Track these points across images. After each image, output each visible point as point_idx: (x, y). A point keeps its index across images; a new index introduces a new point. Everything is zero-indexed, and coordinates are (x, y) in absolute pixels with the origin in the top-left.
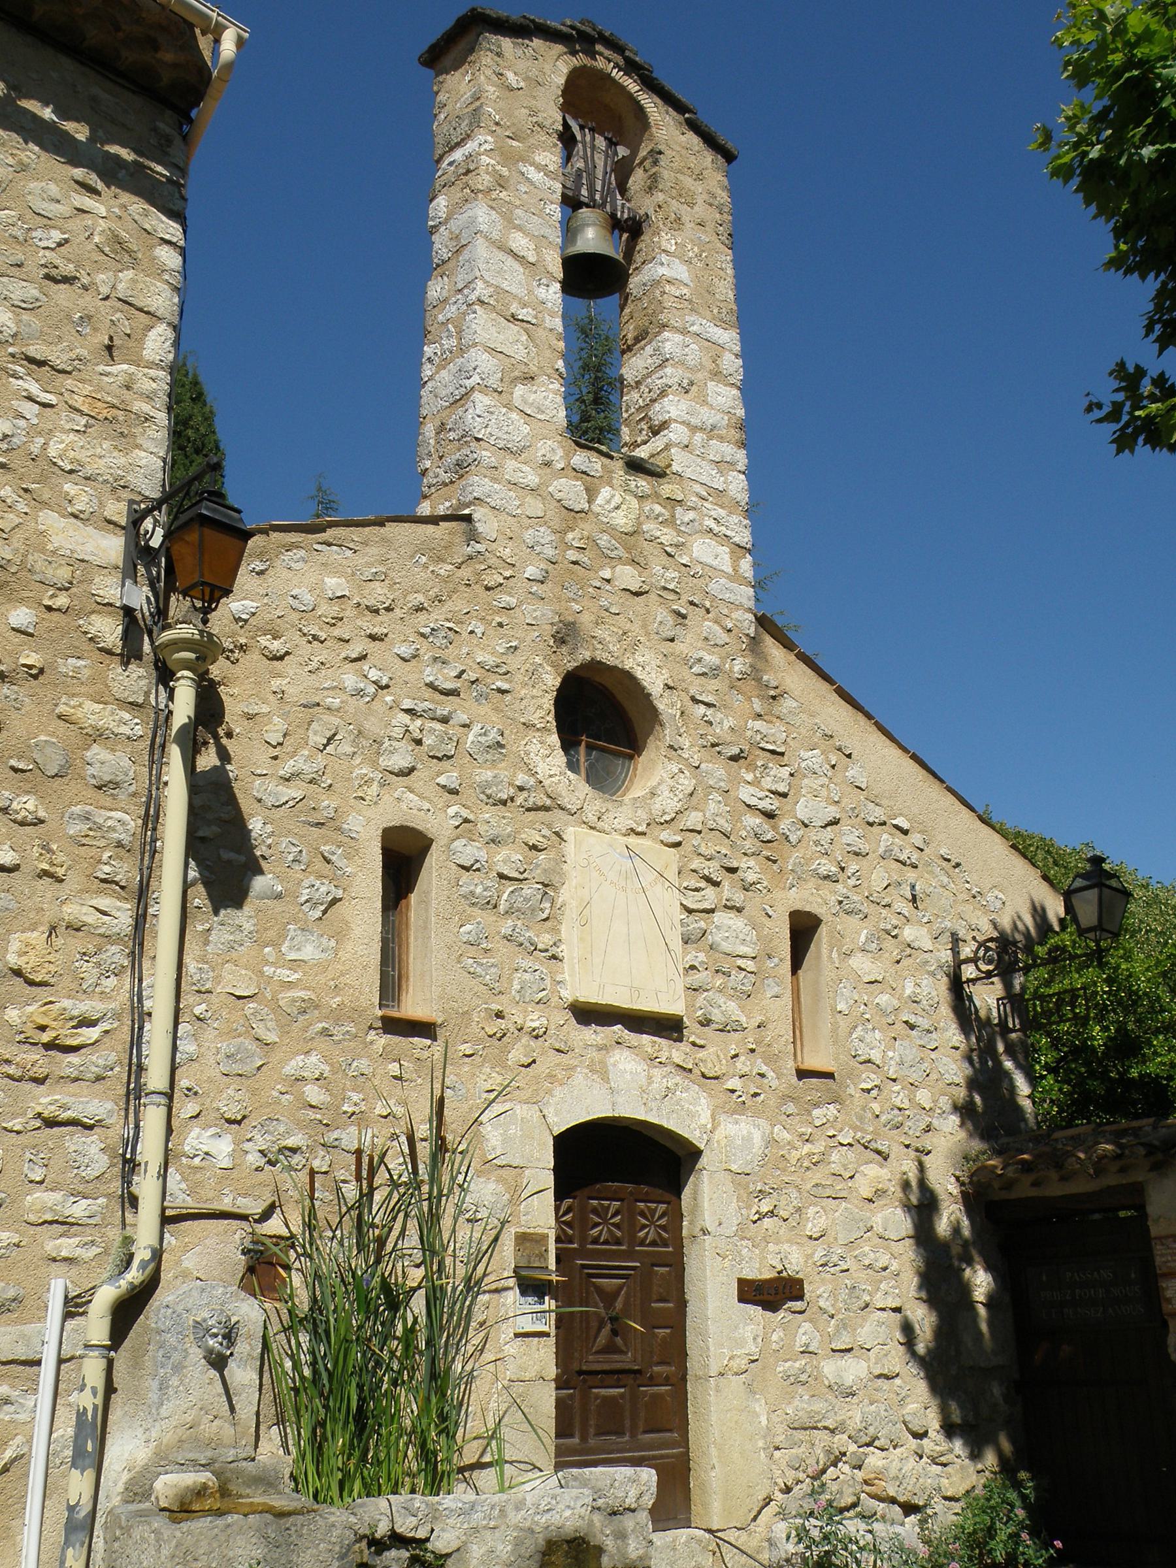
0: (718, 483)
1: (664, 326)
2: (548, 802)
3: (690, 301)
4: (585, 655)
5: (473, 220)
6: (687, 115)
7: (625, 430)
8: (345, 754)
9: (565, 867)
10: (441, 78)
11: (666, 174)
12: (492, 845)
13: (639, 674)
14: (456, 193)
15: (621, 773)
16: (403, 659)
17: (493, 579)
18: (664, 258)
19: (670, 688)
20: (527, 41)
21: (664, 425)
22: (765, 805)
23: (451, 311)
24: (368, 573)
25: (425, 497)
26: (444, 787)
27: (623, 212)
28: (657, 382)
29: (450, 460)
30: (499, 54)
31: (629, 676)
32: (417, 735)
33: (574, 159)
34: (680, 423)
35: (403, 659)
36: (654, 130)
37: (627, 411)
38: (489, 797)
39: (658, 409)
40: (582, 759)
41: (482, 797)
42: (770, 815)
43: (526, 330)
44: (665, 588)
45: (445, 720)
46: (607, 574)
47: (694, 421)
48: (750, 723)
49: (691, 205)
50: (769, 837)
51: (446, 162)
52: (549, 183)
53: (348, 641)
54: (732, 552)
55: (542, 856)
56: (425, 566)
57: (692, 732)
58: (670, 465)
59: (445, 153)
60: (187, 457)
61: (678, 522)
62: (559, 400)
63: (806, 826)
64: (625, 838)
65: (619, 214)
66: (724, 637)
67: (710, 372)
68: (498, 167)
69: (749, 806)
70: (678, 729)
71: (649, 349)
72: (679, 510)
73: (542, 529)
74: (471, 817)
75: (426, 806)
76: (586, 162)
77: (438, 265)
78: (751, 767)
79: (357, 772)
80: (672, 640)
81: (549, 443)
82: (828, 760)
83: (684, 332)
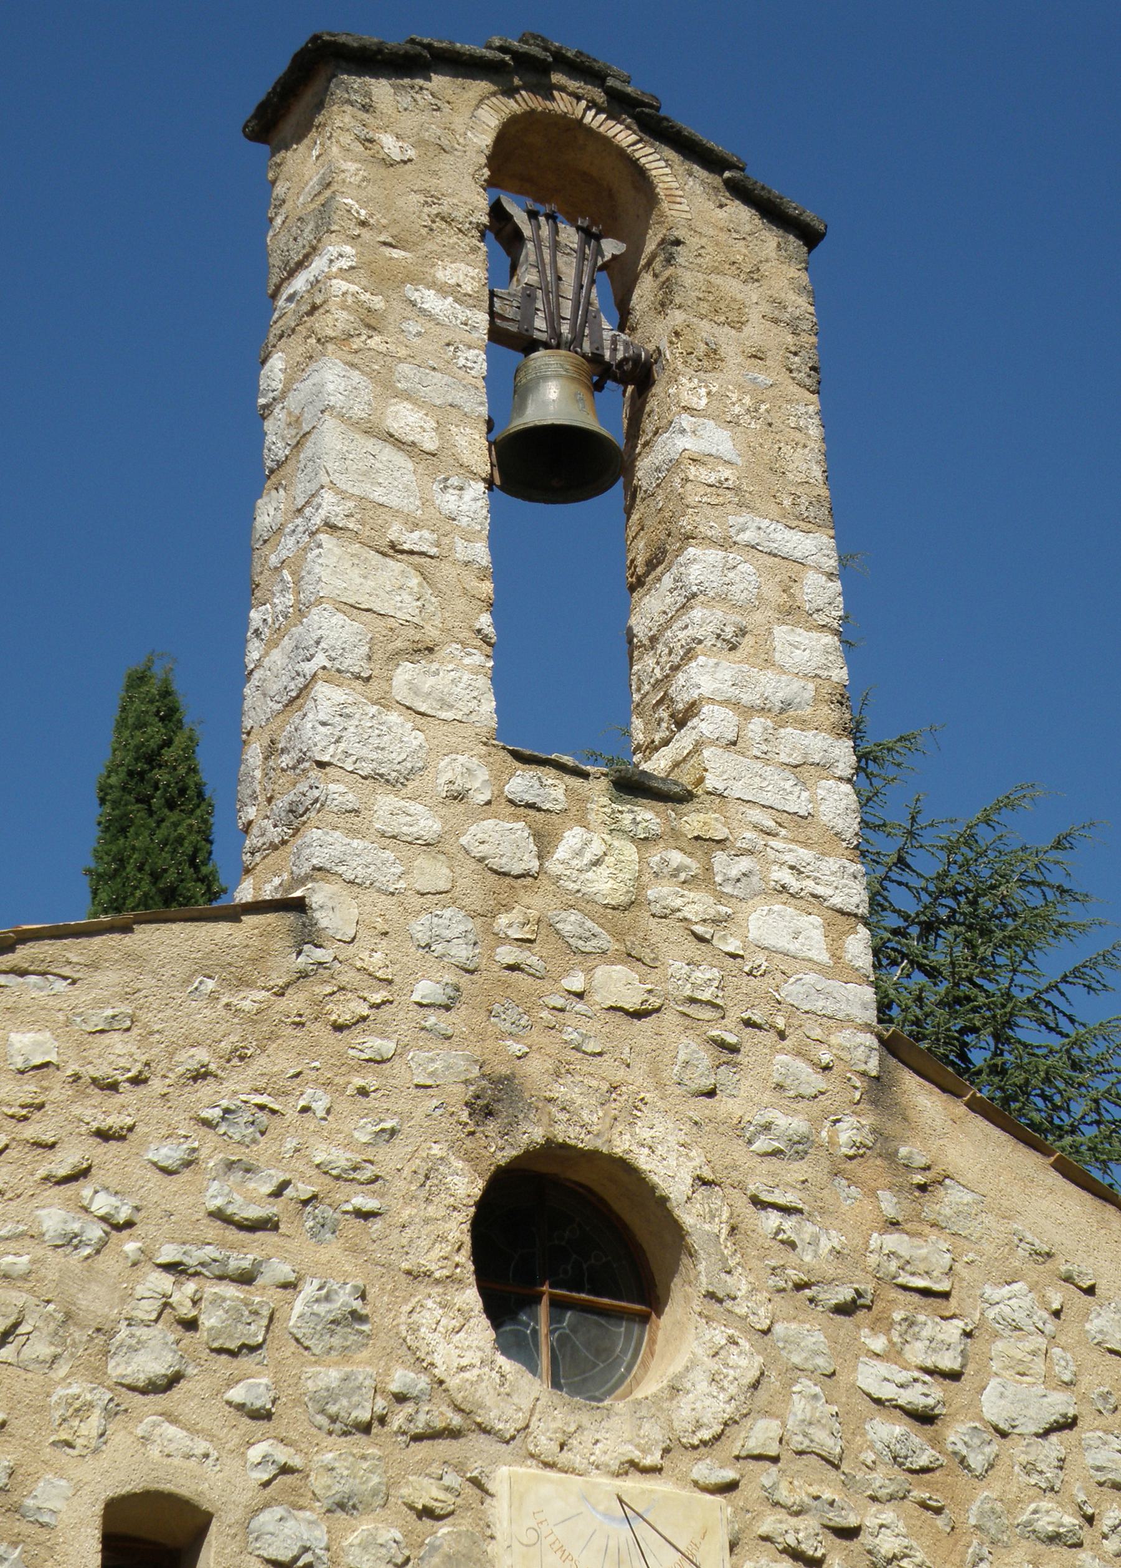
0: (799, 803)
1: (688, 537)
2: (456, 1420)
3: (736, 490)
4: (533, 1134)
5: (319, 390)
6: (727, 174)
7: (637, 723)
8: (37, 1360)
9: (491, 1548)
10: (277, 159)
11: (687, 278)
12: (340, 1514)
13: (643, 1161)
14: (297, 346)
15: (624, 1351)
16: (167, 1171)
17: (347, 1009)
18: (686, 421)
19: (706, 1183)
20: (420, 82)
21: (692, 709)
22: (913, 1397)
23: (288, 546)
24: (97, 1021)
25: (247, 871)
26: (240, 1407)
27: (614, 350)
28: (679, 636)
29: (281, 803)
30: (366, 108)
31: (624, 1168)
32: (186, 1311)
33: (521, 270)
34: (720, 703)
35: (167, 1171)
36: (665, 205)
37: (639, 690)
38: (333, 1419)
39: (681, 682)
40: (543, 1329)
41: (322, 1420)
42: (924, 1418)
43: (419, 569)
44: (693, 1001)
45: (246, 1278)
46: (576, 982)
47: (746, 698)
48: (875, 1240)
49: (738, 325)
50: (923, 1461)
51: (284, 297)
52: (463, 313)
53: (52, 1146)
54: (828, 925)
55: (444, 1529)
56: (213, 997)
57: (754, 1263)
58: (701, 780)
59: (283, 281)
60: (151, 813)
61: (718, 879)
62: (483, 683)
63: (1004, 1435)
64: (618, 1482)
65: (607, 355)
66: (815, 1081)
67: (779, 609)
68: (365, 297)
69: (878, 1401)
70: (724, 1259)
71: (667, 581)
72: (720, 858)
73: (447, 913)
74: (297, 1461)
75: (201, 1446)
76: (542, 273)
77: (272, 471)
78: (882, 1324)
79: (61, 1392)
80: (711, 1094)
81: (461, 759)
82: (1044, 1303)
83: (726, 544)
